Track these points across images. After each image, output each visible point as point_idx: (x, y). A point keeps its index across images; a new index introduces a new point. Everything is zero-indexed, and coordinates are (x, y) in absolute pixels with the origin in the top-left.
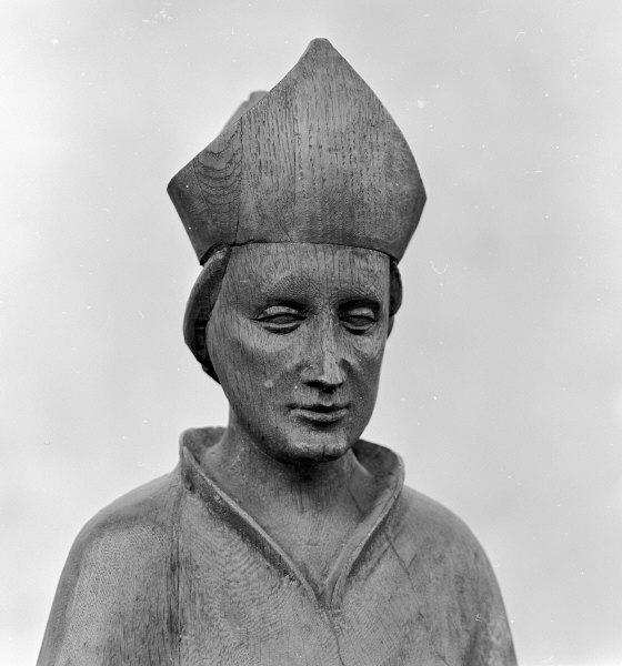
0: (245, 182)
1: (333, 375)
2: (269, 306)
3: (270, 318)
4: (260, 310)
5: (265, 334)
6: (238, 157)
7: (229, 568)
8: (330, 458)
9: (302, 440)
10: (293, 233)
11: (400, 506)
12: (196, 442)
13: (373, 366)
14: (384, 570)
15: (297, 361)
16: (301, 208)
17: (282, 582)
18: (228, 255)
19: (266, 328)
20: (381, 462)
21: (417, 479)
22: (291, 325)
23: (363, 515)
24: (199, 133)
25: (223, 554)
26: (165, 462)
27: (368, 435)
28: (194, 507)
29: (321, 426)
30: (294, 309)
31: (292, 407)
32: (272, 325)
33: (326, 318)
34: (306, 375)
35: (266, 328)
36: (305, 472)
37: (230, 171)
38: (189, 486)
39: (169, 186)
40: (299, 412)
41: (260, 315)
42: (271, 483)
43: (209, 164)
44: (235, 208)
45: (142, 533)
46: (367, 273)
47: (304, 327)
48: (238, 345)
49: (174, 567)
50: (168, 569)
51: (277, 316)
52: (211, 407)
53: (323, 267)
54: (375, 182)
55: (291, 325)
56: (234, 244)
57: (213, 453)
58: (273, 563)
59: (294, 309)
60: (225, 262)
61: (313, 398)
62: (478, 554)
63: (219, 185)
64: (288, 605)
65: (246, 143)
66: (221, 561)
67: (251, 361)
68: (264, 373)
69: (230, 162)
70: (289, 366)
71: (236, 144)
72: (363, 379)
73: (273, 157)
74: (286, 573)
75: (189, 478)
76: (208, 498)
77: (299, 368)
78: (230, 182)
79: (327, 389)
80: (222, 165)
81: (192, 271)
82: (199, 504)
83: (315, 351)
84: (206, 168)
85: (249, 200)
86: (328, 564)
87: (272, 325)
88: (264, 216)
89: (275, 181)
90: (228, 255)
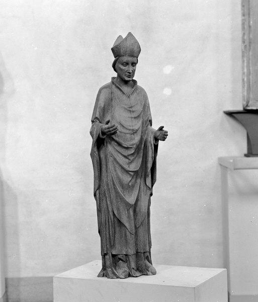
1: (131, 71)
8: (129, 81)
9: (127, 79)
11: (137, 87)
12: (113, 78)
13: (135, 70)
14: (135, 94)
16: (128, 52)
20: (135, 82)
21: (139, 84)
23: (133, 88)
24: (112, 47)
26: (110, 81)
27: (134, 78)
28: (114, 86)
29: (129, 77)
30: (127, 64)
33: (130, 65)
36: (126, 82)
39: (91, 154)
41: (123, 64)
45: (108, 89)
46: (134, 60)
48: (120, 68)
52: (115, 75)
53: (130, 59)
54: (136, 49)
57: (115, 80)
59: (127, 64)
61: (128, 74)
62: (146, 93)
64: (124, 97)
67: (121, 70)
72: (134, 72)
75: (113, 83)
76: (115, 85)
79: (130, 73)
81: (113, 59)
83: (151, 274)
85: (122, 51)
86: (137, 156)
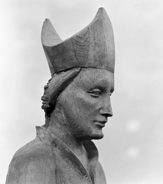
0: (90, 48)
2: (95, 88)
3: (93, 92)
4: (92, 89)
5: (90, 97)
6: (88, 40)
7: (70, 173)
10: (103, 67)
15: (99, 107)
17: (83, 177)
18: (80, 71)
19: (91, 95)
22: (98, 95)
25: (68, 168)
31: (95, 121)
32: (94, 95)
34: (102, 112)
35: (91, 95)
37: (85, 44)
38: (54, 145)
40: (97, 123)
42: (72, 146)
43: (78, 40)
44: (86, 56)
47: (101, 97)
49: (56, 172)
50: (55, 173)
51: (97, 92)
55: (98, 95)
56: (83, 67)
58: (81, 171)
60: (78, 72)
63: (81, 47)
65: (91, 36)
66: (67, 170)
68: (89, 110)
69: (86, 41)
70: (97, 108)
71: (87, 36)
73: (99, 42)
74: (85, 174)
77: (100, 109)
78: (85, 47)
80: (82, 41)
82: (59, 151)
84: (77, 42)
87: (94, 95)
88: (96, 60)
89: (100, 50)
90: (80, 71)
